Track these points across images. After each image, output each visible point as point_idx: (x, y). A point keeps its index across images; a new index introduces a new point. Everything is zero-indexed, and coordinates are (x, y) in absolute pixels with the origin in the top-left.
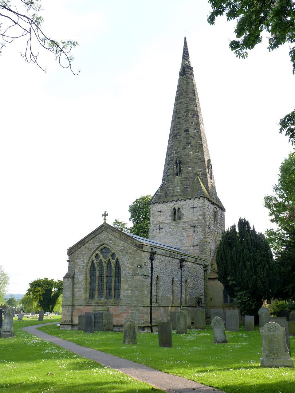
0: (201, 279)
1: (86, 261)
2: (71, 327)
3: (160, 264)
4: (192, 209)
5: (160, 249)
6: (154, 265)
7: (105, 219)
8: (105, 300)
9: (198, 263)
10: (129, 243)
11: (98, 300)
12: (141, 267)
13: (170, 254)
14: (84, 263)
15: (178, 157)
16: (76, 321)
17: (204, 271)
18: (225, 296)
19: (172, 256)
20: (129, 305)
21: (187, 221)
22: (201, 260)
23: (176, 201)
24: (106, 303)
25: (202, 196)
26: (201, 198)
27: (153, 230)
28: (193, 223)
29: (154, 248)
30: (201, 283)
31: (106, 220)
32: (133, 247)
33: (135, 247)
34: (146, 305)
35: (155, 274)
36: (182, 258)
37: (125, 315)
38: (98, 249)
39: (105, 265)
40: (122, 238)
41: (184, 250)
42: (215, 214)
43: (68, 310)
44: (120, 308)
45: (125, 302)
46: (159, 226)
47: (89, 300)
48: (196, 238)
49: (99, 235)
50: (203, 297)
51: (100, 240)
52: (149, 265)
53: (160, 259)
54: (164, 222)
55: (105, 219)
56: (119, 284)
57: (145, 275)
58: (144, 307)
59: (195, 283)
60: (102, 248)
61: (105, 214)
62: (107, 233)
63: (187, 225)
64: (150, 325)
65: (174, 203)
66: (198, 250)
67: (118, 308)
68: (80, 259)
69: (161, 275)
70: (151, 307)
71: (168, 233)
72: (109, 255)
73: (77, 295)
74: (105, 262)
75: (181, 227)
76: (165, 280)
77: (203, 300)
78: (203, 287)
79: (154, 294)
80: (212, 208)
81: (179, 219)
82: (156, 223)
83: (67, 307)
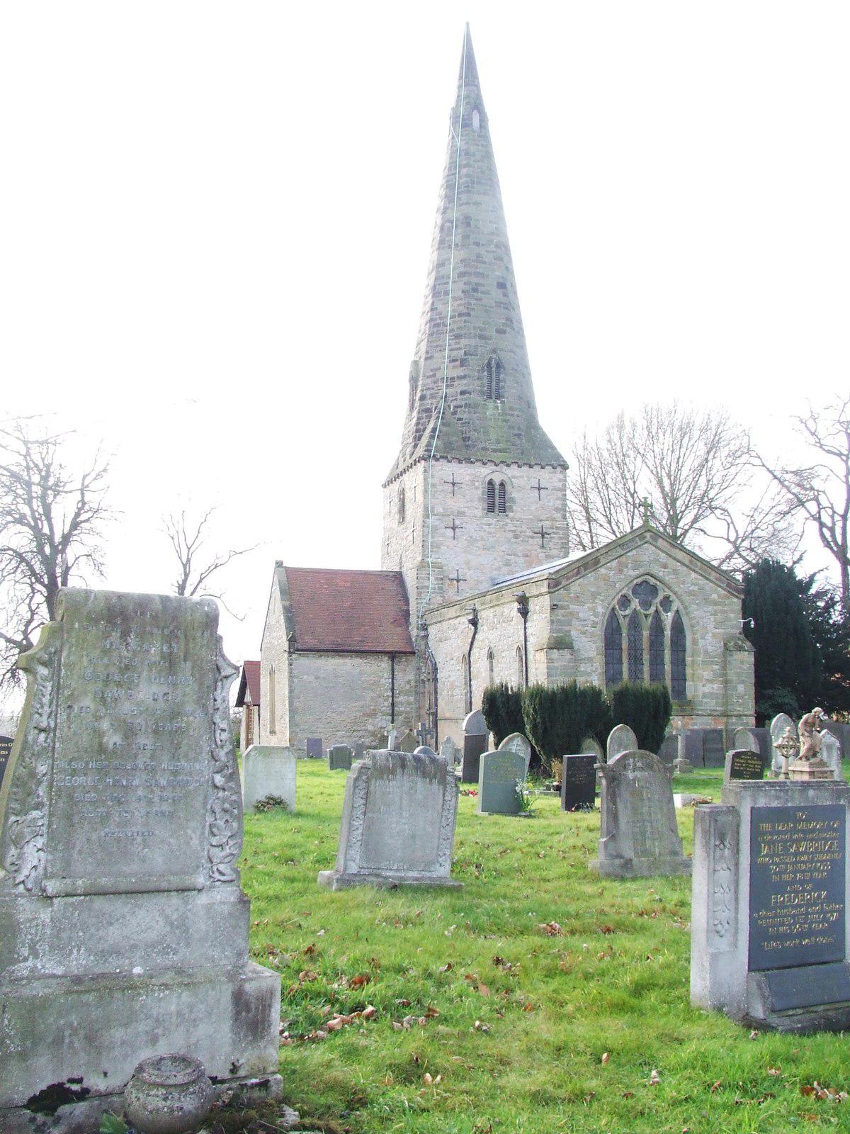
14: (596, 615)
71: (476, 540)
81: (503, 510)
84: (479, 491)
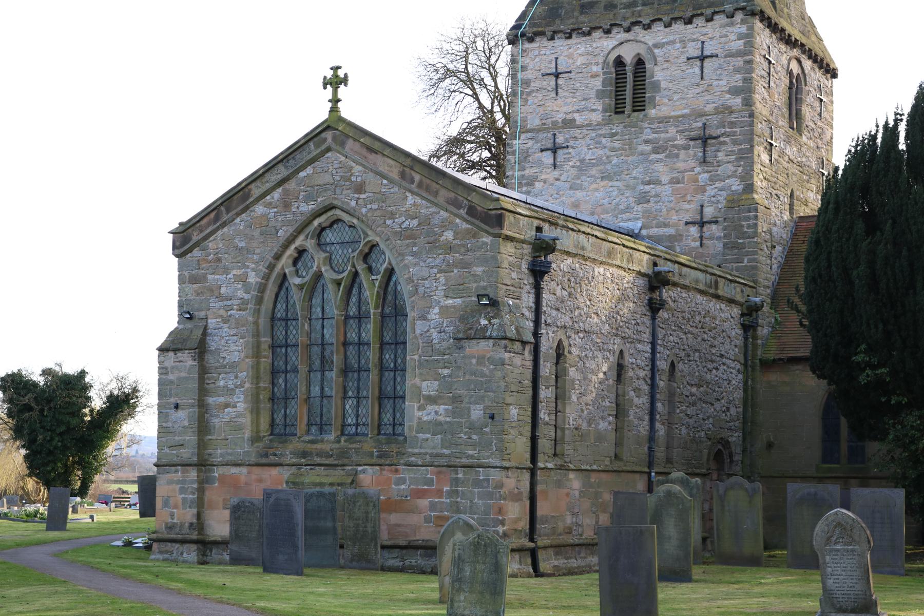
0: (728, 362)
1: (253, 278)
2: (198, 549)
3: (570, 294)
4: (698, 63)
5: (570, 232)
6: (545, 296)
7: (335, 101)
8: (339, 442)
9: (720, 292)
10: (441, 200)
11: (312, 442)
12: (494, 303)
13: (610, 254)
16: (219, 526)
17: (746, 328)
18: (830, 433)
19: (618, 263)
20: (443, 461)
21: (673, 114)
22: (731, 281)
23: (628, 30)
24: (343, 454)
25: (743, 9)
26: (739, 16)
27: (526, 155)
28: (700, 124)
29: (546, 227)
30: (731, 376)
31: (340, 104)
32: (458, 220)
33: (469, 218)
34: (513, 464)
35: (551, 335)
36: (659, 273)
37: (424, 503)
38: (307, 231)
40: (412, 182)
42: (795, 88)
43: (183, 482)
44: (406, 473)
45: (423, 451)
46: (550, 135)
47: (271, 441)
48: (710, 191)
49: (309, 170)
50: (735, 438)
52: (524, 296)
54: (574, 120)
55: (335, 101)
56: (399, 379)
57: (511, 340)
58: (507, 468)
59: (708, 376)
60: (324, 225)
61: (336, 76)
62: (343, 158)
63: (672, 131)
64: (532, 545)
65: (619, 35)
66: (719, 238)
67: (394, 477)
68: (226, 271)
69: (577, 339)
72: (355, 254)
74: (338, 283)
75: (647, 142)
77: (737, 450)
78: (739, 395)
79: (547, 419)
80: (782, 56)
81: (639, 105)
82: (537, 122)
83: (176, 471)
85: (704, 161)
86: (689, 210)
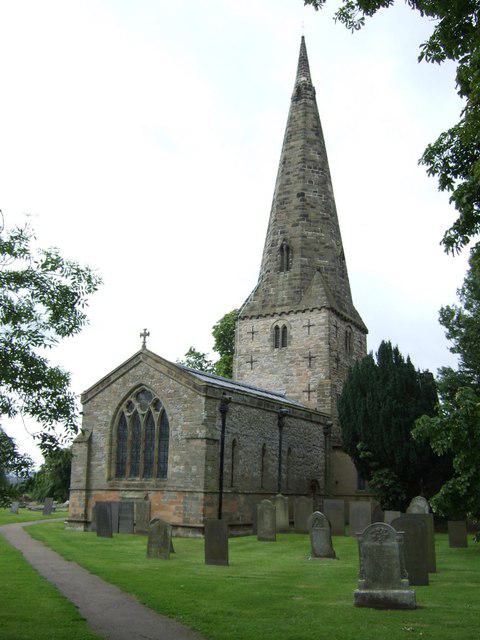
1: (111, 413)
6: (227, 421)
15: (284, 240)
17: (325, 434)
26: (323, 310)
37: (173, 507)
39: (142, 420)
41: (292, 398)
42: (348, 337)
51: (135, 378)
53: (240, 411)
63: (297, 355)
68: (101, 410)
69: (242, 438)
70: (221, 493)
73: (95, 471)
74: (143, 415)
76: (250, 446)
77: (322, 485)
78: (323, 461)
80: (342, 326)
81: (284, 344)
84: (268, 335)
85: (310, 366)
86: (304, 386)
